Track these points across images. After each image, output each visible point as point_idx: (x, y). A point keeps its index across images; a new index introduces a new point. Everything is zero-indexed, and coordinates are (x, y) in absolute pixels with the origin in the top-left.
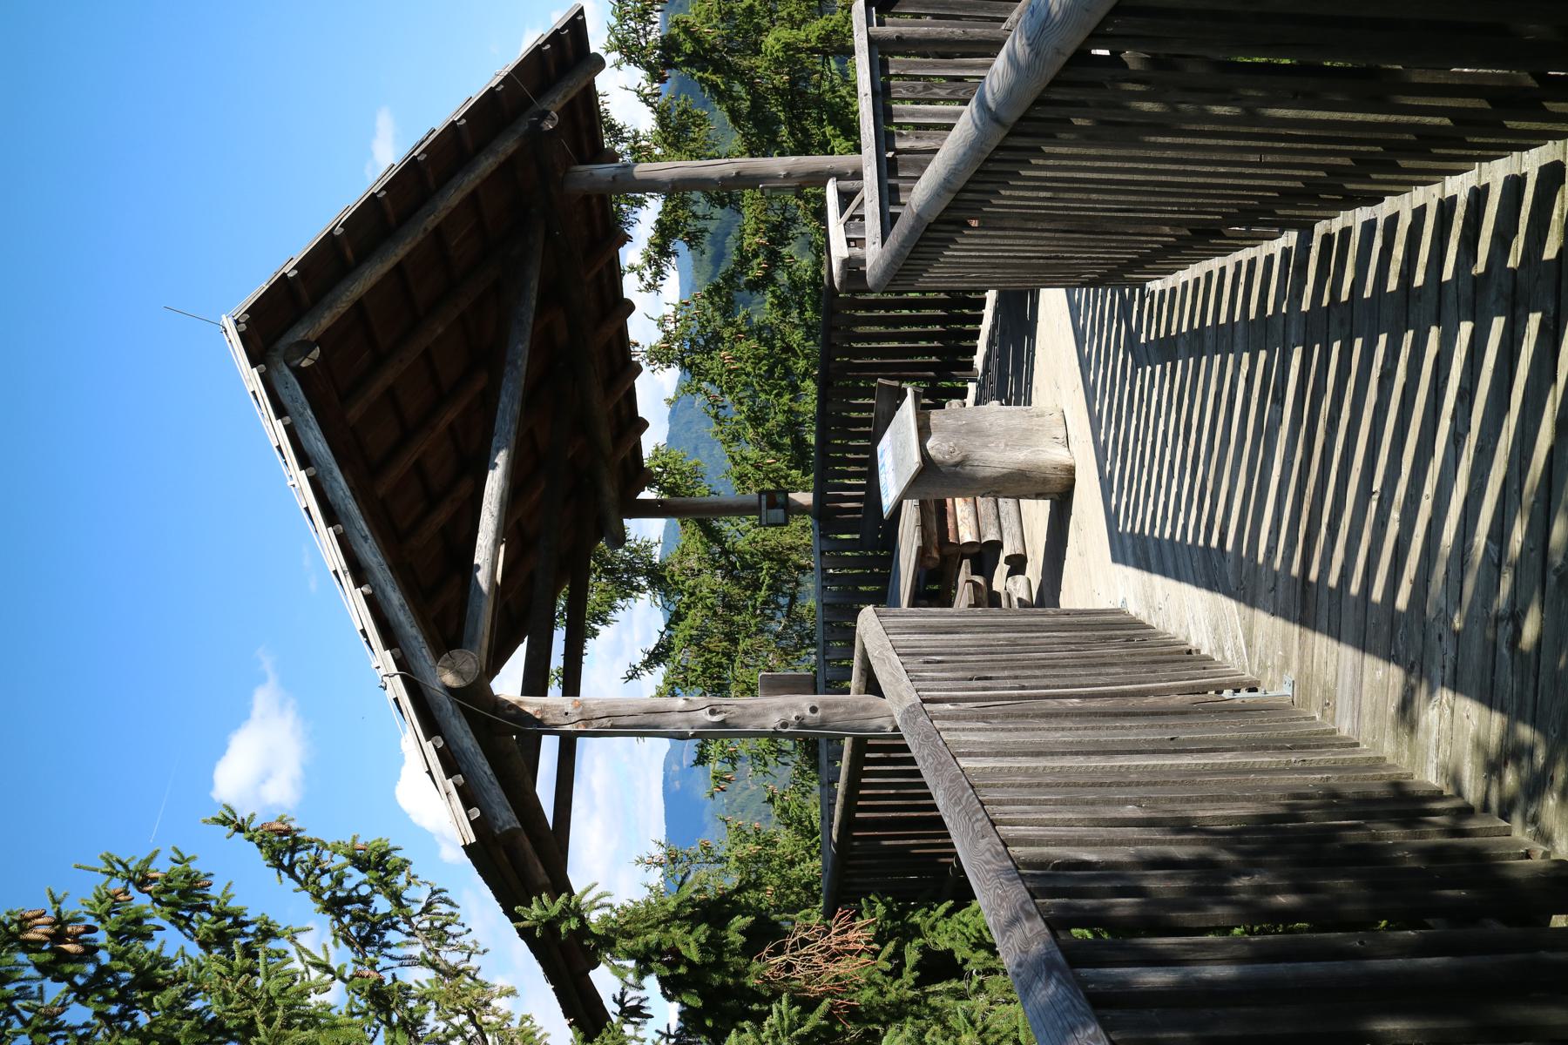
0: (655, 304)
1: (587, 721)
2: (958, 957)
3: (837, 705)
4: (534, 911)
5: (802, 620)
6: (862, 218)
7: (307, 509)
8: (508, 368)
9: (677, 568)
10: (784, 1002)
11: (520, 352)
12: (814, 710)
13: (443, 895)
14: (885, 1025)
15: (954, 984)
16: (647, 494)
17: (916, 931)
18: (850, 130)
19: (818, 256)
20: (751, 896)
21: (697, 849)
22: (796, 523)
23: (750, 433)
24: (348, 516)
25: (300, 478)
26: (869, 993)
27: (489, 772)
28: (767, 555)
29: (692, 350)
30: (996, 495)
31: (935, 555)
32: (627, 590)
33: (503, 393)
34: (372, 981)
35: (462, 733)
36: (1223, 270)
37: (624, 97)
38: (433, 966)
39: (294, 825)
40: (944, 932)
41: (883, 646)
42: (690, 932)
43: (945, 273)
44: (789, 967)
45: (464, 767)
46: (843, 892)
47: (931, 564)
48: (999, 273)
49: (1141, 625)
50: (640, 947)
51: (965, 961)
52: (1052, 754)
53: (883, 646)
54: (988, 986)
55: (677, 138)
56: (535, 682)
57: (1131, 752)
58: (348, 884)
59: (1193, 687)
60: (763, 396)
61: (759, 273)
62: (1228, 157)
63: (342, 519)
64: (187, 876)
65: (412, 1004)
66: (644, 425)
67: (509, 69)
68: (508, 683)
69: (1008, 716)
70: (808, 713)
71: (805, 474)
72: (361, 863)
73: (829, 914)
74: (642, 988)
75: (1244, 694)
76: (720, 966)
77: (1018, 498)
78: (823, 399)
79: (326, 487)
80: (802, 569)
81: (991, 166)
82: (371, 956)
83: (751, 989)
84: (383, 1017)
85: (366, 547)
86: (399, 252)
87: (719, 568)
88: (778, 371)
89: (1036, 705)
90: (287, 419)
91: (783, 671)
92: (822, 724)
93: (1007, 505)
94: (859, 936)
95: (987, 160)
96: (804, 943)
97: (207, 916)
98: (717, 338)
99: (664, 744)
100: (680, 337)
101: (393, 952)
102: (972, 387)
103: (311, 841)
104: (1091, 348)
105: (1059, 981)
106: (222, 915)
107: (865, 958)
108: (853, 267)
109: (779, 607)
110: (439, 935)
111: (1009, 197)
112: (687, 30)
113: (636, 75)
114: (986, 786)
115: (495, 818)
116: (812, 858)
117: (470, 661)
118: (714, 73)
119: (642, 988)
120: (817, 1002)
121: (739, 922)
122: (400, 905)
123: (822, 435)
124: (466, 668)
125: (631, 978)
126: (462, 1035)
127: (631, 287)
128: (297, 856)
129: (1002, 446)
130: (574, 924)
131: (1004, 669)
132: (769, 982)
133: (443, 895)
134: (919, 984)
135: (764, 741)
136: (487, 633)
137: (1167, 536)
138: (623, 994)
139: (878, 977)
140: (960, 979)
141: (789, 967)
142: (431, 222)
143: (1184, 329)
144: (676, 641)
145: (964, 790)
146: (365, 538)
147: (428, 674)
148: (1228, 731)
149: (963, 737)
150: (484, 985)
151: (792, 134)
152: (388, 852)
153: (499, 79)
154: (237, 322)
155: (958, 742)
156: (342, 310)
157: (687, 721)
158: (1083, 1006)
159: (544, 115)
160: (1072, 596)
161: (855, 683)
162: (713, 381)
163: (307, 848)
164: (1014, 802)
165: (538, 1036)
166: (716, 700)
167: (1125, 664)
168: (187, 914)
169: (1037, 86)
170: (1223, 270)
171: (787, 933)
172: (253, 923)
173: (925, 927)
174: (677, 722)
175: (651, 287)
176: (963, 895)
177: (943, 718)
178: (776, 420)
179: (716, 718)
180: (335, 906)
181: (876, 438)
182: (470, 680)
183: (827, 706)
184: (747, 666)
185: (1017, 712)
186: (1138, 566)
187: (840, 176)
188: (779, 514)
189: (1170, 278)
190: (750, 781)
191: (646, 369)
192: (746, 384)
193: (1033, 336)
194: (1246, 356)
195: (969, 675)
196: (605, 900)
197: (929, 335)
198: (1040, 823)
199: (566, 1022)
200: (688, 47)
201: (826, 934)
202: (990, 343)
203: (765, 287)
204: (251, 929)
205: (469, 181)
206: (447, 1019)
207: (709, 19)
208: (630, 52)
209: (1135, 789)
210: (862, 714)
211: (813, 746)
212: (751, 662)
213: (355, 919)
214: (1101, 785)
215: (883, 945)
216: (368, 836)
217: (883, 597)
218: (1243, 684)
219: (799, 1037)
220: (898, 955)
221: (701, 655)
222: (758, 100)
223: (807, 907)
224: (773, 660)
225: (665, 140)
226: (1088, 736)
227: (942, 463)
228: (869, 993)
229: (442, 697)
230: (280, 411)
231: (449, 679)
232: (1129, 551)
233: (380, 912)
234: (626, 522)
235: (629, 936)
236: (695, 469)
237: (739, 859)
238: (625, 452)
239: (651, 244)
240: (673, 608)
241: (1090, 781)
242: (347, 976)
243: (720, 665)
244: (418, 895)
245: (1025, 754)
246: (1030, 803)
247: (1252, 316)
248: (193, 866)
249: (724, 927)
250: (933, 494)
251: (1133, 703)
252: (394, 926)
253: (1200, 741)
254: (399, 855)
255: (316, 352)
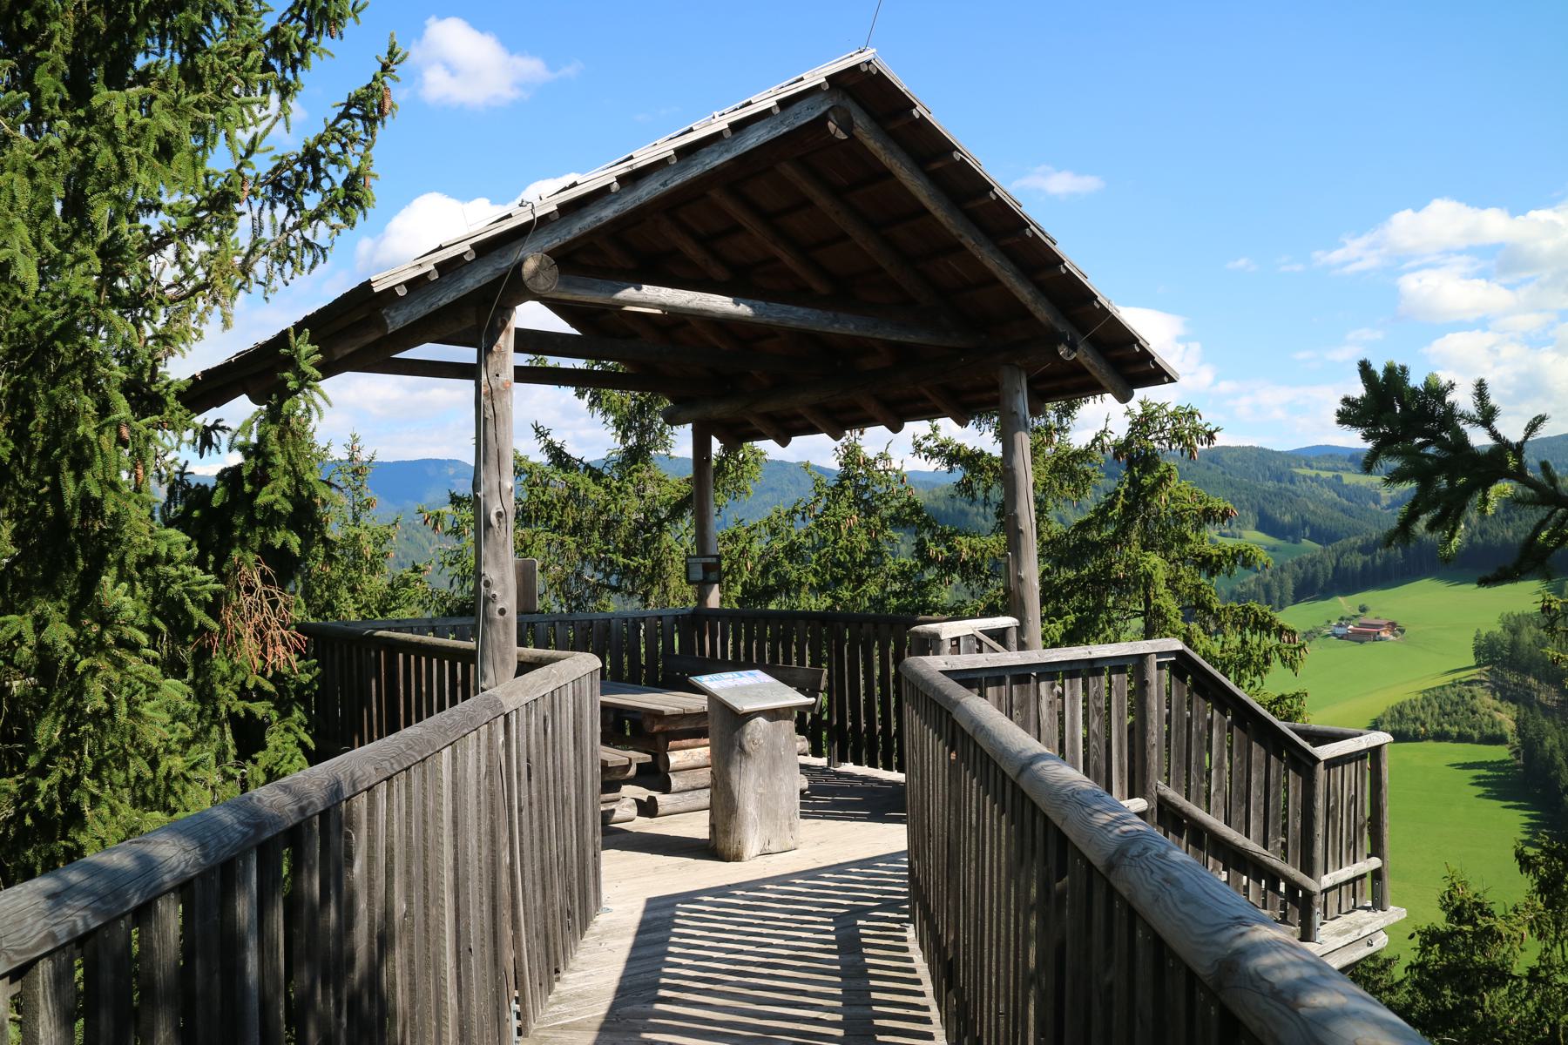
0: (903, 451)
1: (491, 395)
2: (259, 755)
3: (507, 634)
4: (304, 346)
5: (595, 598)
6: (980, 651)
7: (691, 130)
8: (831, 315)
9: (645, 475)
10: (216, 586)
11: (846, 326)
12: (502, 612)
13: (321, 260)
14: (192, 684)
15: (232, 751)
16: (716, 445)
17: (285, 714)
18: (1071, 638)
19: (951, 609)
20: (320, 550)
21: (368, 494)
22: (690, 592)
23: (778, 545)
24: (685, 167)
25: (721, 124)
26: (224, 667)
27: (441, 303)
28: (658, 563)
29: (857, 486)
30: (713, 786)
31: (656, 728)
32: (624, 425)
33: (808, 310)
34: (239, 193)
35: (478, 277)
36: (922, 994)
37: (1099, 419)
38: (253, 250)
39: (387, 119)
40: (281, 741)
41: (561, 677)
42: (284, 494)
43: (916, 731)
44: (250, 590)
45: (445, 280)
46: (323, 642)
47: (647, 724)
48: (916, 781)
49: (585, 925)
50: (270, 448)
51: (255, 762)
52: (455, 836)
53: (561, 677)
54: (230, 784)
55: (1063, 470)
56: (528, 341)
57: (457, 909)
58: (332, 169)
59: (522, 973)
60: (814, 557)
61: (932, 553)
62: (1002, 984)
63: (682, 163)
64: (340, 16)
65: (216, 229)
66: (784, 442)
67: (1114, 313)
68: (532, 315)
69: (492, 795)
70: (499, 606)
71: (738, 600)
72: (351, 182)
73: (302, 628)
74: (230, 450)
75: (516, 1023)
76: (251, 523)
77: (711, 808)
78: (809, 617)
79: (714, 146)
80: (645, 598)
81: (992, 767)
82: (262, 191)
83: (228, 553)
84: (204, 203)
85: (656, 185)
86: (939, 211)
87: (646, 517)
88: (839, 572)
89: (503, 821)
90: (777, 111)
91: (540, 582)
92: (488, 620)
93: (704, 798)
94: (281, 657)
95: (996, 765)
96: (274, 604)
97: (302, 35)
98: (870, 510)
99: (473, 464)
100: (869, 476)
101: (267, 212)
102: (823, 762)
103: (372, 134)
104: (855, 874)
105: (244, 834)
106: (303, 49)
107: (259, 663)
108: (930, 644)
109: (607, 576)
110: (282, 255)
111: (972, 785)
112: (1162, 479)
113: (1120, 430)
114: (424, 773)
115: (397, 309)
116: (358, 610)
117: (548, 282)
118: (1124, 505)
119: (230, 450)
120: (216, 617)
121: (295, 542)
122: (311, 219)
123: (778, 616)
124: (541, 280)
125: (240, 439)
126: (185, 278)
127: (916, 429)
128: (359, 122)
129: (760, 790)
130: (292, 385)
131: (539, 792)
132: (236, 570)
133: (321, 260)
134: (233, 717)
135: (472, 562)
136: (576, 298)
137: (671, 949)
138: (223, 429)
139: (239, 676)
140: (236, 758)
141: (250, 590)
142: (968, 241)
143: (868, 960)
144: (573, 474)
145: (421, 753)
146: (664, 184)
147: (535, 245)
148: (479, 1005)
149: (471, 752)
150: (233, 297)
151: (1068, 582)
152: (362, 207)
153: (1105, 304)
154: (869, 63)
155: (466, 748)
156: (882, 159)
157: (491, 491)
158: (225, 854)
159: (1073, 347)
160: (614, 863)
161: (531, 651)
162: (827, 508)
163: (366, 131)
164: (409, 798)
165: (183, 346)
166: (511, 517)
167: (545, 909)
168: (304, 15)
169: (1042, 803)
170: (922, 994)
171: (283, 587)
172: (295, 77)
173: (287, 722)
174: (489, 481)
175: (918, 446)
176: (314, 758)
177: (490, 735)
178: (791, 570)
179: (493, 518)
180: (311, 157)
181: (761, 666)
182: (529, 284)
183: (506, 624)
184: (549, 545)
185: (496, 804)
186: (643, 923)
187: (1021, 630)
188: (698, 574)
189: (917, 946)
190: (438, 546)
191: (838, 444)
192: (826, 540)
193: (870, 819)
194: (839, 1017)
195: (533, 759)
196: (315, 413)
197: (866, 719)
198: (389, 822)
199: (198, 373)
200: (1147, 481)
201: (282, 625)
202: (865, 779)
203: (920, 557)
204: (289, 75)
205: (1008, 277)
206: (201, 263)
207: (1174, 500)
208: (1143, 423)
209: (421, 912)
210: (498, 658)
211: (468, 612)
212: (552, 549)
213: (298, 176)
214: (426, 880)
215: (271, 680)
216: (377, 189)
217: (612, 678)
218: (525, 1022)
219: (182, 600)
220: (262, 695)
221: (558, 501)
222: (1098, 548)
223: (308, 606)
224: (555, 570)
225: (1060, 458)
226: (473, 871)
227: (743, 733)
228: (224, 667)
229: (514, 258)
230: (784, 104)
231: (530, 265)
232: (657, 914)
233: (305, 199)
234: (689, 426)
235: (281, 437)
236: (744, 491)
237: (357, 536)
238: (757, 425)
239: (960, 447)
240: (606, 471)
241: (429, 870)
242: (244, 170)
243: (550, 518)
244: (320, 233)
245: (455, 811)
246: (408, 814)
247: (876, 1022)
248: (349, 21)
249: (289, 527)
250: (713, 725)
251: (506, 914)
252: (291, 212)
253: (468, 977)
254: (359, 217)
255: (842, 136)
